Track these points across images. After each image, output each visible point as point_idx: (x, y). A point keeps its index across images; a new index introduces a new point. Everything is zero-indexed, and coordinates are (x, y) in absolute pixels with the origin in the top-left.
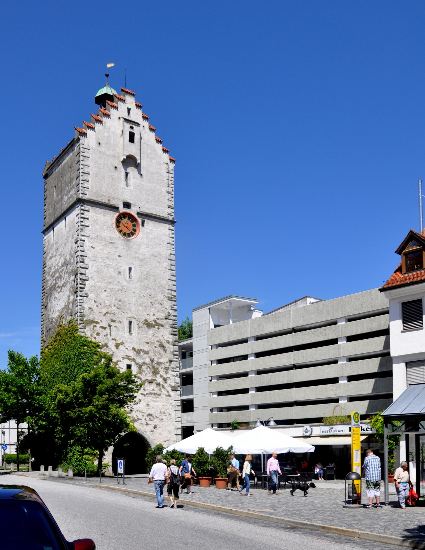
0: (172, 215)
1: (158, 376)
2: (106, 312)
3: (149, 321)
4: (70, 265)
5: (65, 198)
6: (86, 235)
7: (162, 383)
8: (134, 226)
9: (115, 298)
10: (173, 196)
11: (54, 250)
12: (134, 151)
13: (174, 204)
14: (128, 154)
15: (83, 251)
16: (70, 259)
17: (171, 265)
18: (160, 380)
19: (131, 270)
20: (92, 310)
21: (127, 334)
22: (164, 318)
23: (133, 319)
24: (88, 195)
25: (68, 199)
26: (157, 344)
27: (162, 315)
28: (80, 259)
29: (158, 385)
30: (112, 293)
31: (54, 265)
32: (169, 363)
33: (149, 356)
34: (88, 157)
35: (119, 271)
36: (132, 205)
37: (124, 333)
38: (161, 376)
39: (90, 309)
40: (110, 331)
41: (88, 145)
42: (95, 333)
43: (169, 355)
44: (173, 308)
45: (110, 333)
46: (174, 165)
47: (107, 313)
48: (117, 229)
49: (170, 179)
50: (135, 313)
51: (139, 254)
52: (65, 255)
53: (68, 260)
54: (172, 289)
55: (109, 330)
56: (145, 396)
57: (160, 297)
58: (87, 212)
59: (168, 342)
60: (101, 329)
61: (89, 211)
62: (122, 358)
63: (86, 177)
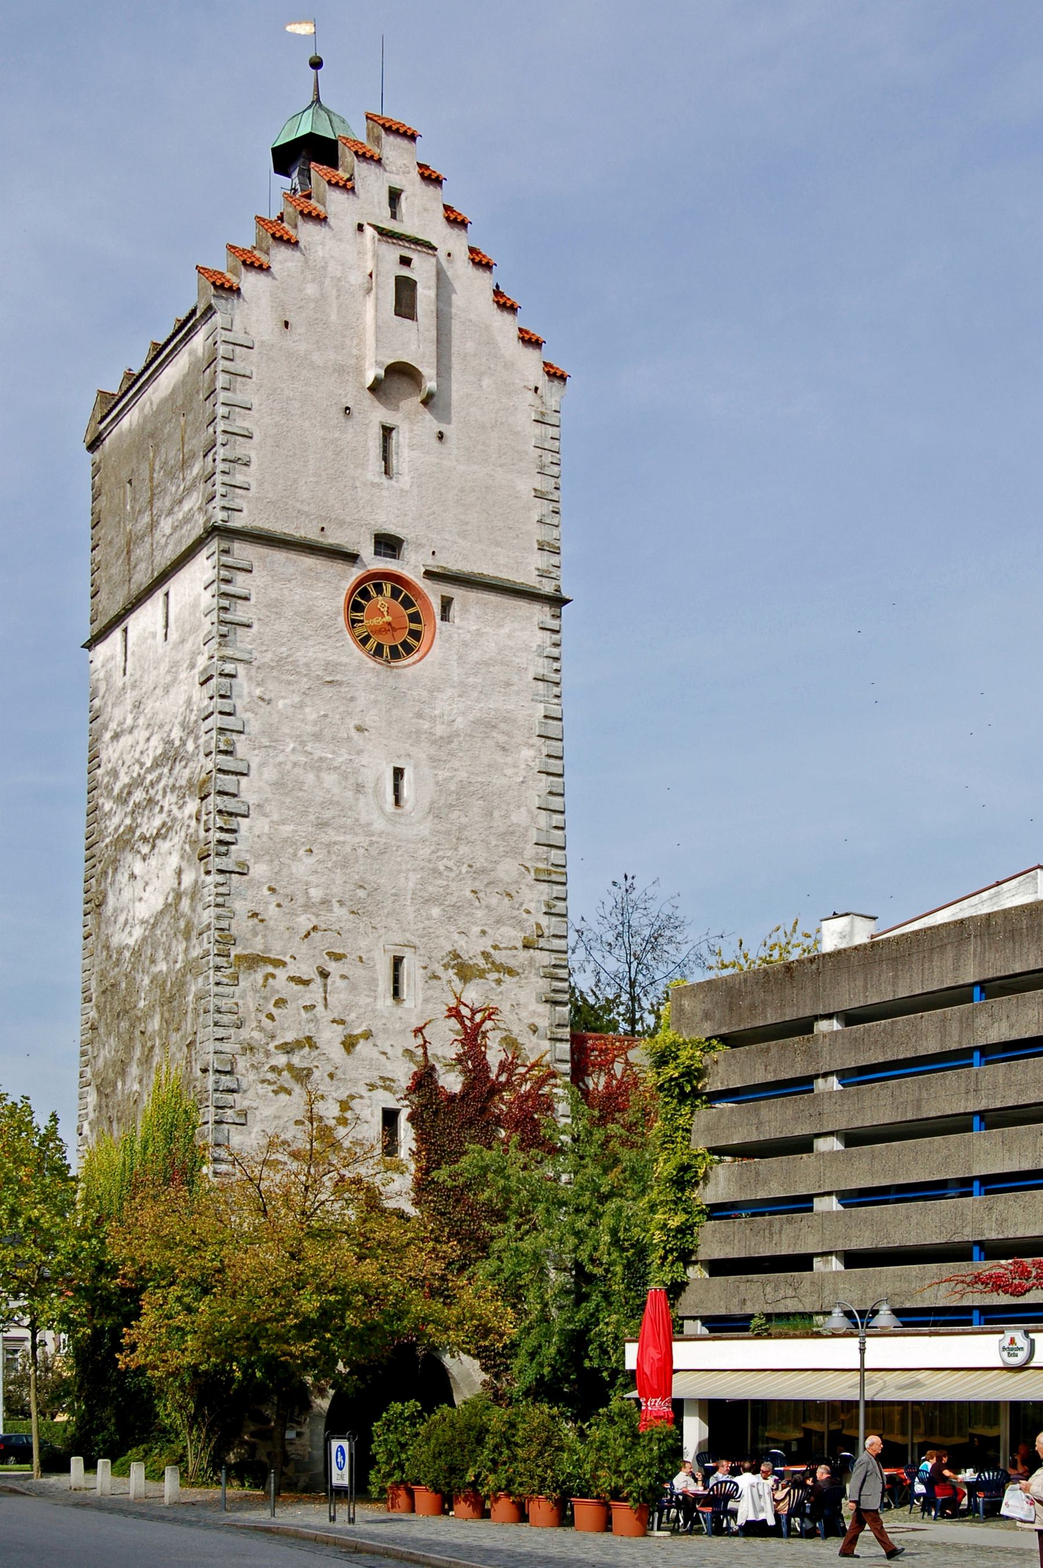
3: (465, 957)
4: (183, 763)
5: (166, 525)
6: (238, 656)
11: (129, 707)
16: (183, 743)
22: (519, 945)
23: (406, 949)
25: (175, 529)
27: (516, 937)
31: (128, 763)
40: (325, 992)
42: (273, 1002)
44: (553, 911)
45: (326, 999)
47: (315, 928)
51: (433, 719)
52: (167, 728)
53: (177, 743)
55: (321, 990)
58: (243, 573)
59: (534, 1030)
60: (292, 984)
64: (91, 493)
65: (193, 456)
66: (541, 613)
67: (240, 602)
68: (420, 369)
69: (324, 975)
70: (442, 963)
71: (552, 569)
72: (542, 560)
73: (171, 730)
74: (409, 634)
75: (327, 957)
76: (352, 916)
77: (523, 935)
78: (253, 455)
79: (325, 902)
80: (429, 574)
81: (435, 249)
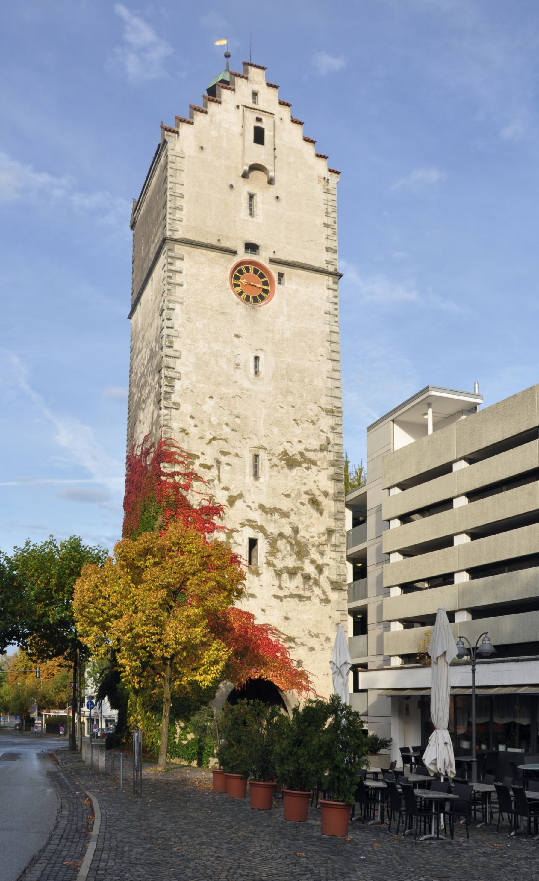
0: (334, 263)
1: (307, 562)
2: (212, 437)
3: (290, 454)
6: (176, 300)
7: (313, 576)
8: (265, 283)
9: (229, 412)
10: (336, 231)
12: (263, 157)
13: (337, 246)
14: (252, 163)
15: (172, 328)
17: (333, 351)
18: (310, 569)
20: (187, 434)
21: (249, 479)
22: (318, 448)
23: (260, 450)
24: (180, 232)
26: (305, 499)
27: (315, 444)
28: (166, 341)
29: (307, 578)
30: (224, 402)
32: (326, 535)
33: (291, 521)
34: (180, 170)
35: (237, 362)
37: (245, 476)
38: (313, 562)
39: (183, 431)
40: (219, 473)
41: (182, 151)
43: (328, 519)
44: (335, 431)
45: (219, 476)
46: (338, 180)
47: (214, 438)
48: (234, 290)
49: (330, 203)
50: (265, 438)
54: (334, 395)
56: (281, 601)
57: (312, 410)
59: (326, 494)
61: (182, 259)
62: (241, 524)
63: (179, 202)
65: (160, 210)
66: (328, 280)
67: (177, 274)
68: (266, 167)
69: (218, 462)
70: (279, 457)
71: (333, 260)
75: (219, 454)
76: (233, 432)
77: (320, 443)
78: (185, 206)
79: (218, 424)
80: (272, 261)
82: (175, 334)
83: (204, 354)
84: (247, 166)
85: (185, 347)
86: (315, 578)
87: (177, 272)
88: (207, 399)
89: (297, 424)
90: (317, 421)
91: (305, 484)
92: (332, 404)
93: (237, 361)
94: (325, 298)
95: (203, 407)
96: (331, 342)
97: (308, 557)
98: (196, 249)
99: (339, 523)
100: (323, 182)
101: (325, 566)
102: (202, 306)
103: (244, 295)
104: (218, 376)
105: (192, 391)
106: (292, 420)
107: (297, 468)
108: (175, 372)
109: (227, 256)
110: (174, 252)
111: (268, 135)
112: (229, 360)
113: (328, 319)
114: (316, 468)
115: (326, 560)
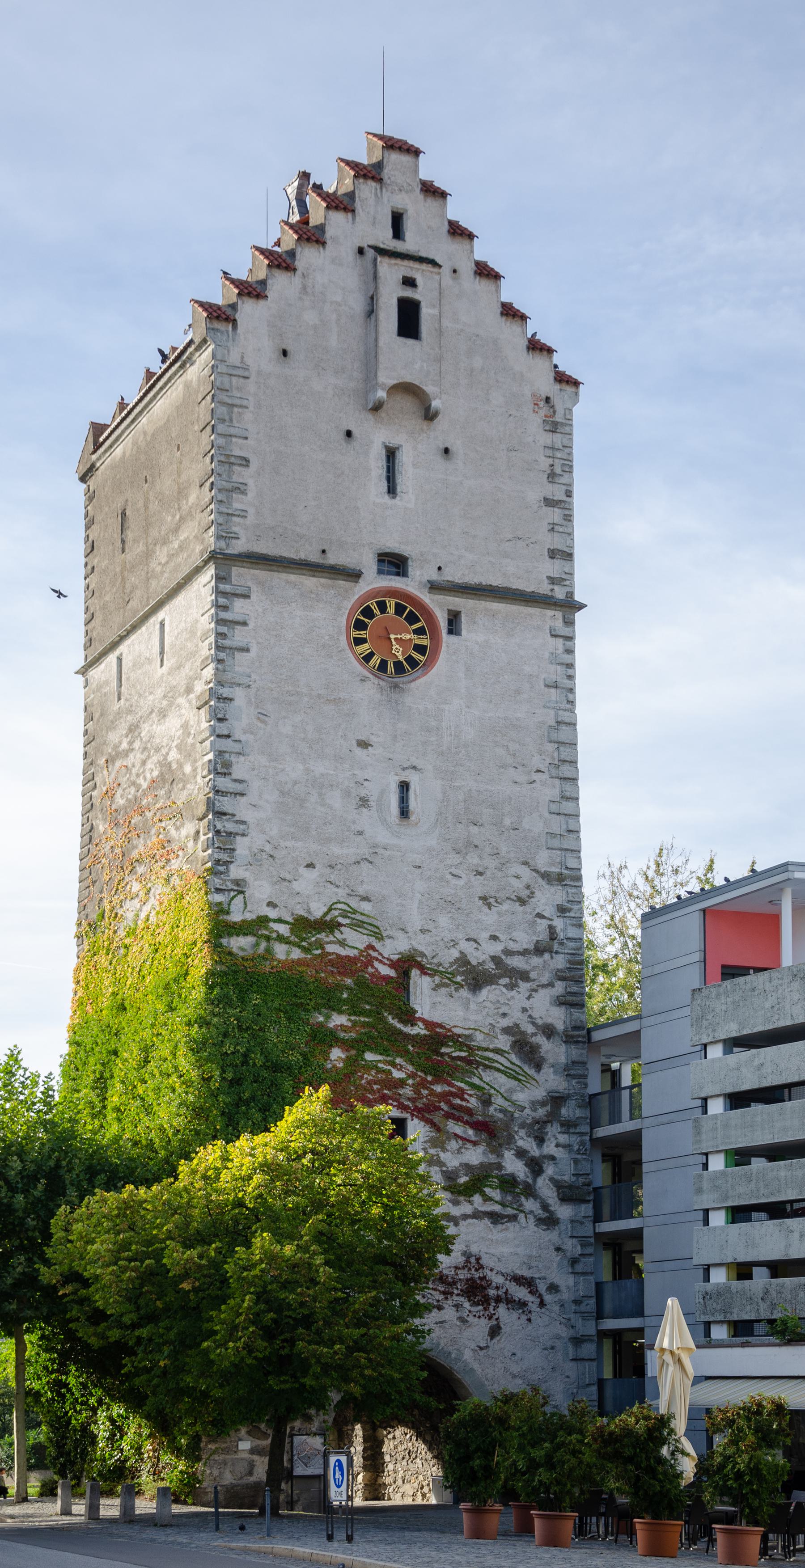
3: (474, 963)
4: (180, 786)
5: (162, 554)
6: (237, 680)
15: (228, 736)
16: (181, 766)
18: (514, 1166)
19: (408, 790)
22: (532, 947)
25: (171, 556)
27: (524, 939)
29: (509, 1183)
34: (241, 406)
36: (410, 563)
38: (521, 1154)
48: (353, 652)
49: (559, 455)
52: (164, 751)
53: (174, 766)
58: (241, 600)
64: (84, 522)
68: (424, 388)
71: (564, 576)
72: (555, 568)
73: (167, 754)
74: (414, 649)
77: (535, 938)
78: (251, 482)
80: (434, 587)
81: (440, 266)
82: (237, 747)
83: (295, 783)
84: (383, 389)
85: (256, 772)
86: (525, 1182)
87: (237, 623)
88: (302, 870)
89: (489, 906)
90: (529, 897)
91: (504, 1015)
92: (560, 863)
93: (363, 793)
94: (547, 655)
95: (296, 885)
96: (558, 743)
97: (512, 1146)
98: (276, 574)
99: (574, 1082)
100: (544, 410)
101: (546, 1161)
102: (291, 688)
103: (376, 661)
104: (325, 824)
105: (271, 856)
106: (477, 899)
107: (489, 988)
108: (237, 822)
109: (385, 484)
110: (230, 583)
111: (426, 313)
112: (347, 793)
113: (554, 698)
114: (528, 985)
115: (550, 1148)
